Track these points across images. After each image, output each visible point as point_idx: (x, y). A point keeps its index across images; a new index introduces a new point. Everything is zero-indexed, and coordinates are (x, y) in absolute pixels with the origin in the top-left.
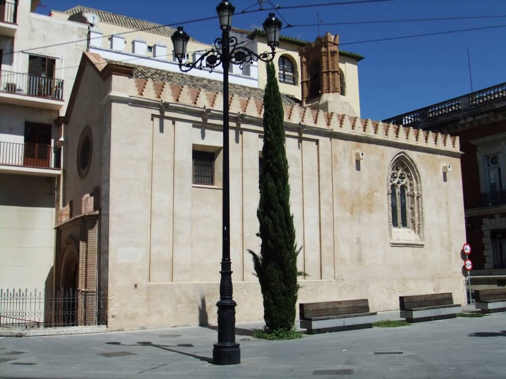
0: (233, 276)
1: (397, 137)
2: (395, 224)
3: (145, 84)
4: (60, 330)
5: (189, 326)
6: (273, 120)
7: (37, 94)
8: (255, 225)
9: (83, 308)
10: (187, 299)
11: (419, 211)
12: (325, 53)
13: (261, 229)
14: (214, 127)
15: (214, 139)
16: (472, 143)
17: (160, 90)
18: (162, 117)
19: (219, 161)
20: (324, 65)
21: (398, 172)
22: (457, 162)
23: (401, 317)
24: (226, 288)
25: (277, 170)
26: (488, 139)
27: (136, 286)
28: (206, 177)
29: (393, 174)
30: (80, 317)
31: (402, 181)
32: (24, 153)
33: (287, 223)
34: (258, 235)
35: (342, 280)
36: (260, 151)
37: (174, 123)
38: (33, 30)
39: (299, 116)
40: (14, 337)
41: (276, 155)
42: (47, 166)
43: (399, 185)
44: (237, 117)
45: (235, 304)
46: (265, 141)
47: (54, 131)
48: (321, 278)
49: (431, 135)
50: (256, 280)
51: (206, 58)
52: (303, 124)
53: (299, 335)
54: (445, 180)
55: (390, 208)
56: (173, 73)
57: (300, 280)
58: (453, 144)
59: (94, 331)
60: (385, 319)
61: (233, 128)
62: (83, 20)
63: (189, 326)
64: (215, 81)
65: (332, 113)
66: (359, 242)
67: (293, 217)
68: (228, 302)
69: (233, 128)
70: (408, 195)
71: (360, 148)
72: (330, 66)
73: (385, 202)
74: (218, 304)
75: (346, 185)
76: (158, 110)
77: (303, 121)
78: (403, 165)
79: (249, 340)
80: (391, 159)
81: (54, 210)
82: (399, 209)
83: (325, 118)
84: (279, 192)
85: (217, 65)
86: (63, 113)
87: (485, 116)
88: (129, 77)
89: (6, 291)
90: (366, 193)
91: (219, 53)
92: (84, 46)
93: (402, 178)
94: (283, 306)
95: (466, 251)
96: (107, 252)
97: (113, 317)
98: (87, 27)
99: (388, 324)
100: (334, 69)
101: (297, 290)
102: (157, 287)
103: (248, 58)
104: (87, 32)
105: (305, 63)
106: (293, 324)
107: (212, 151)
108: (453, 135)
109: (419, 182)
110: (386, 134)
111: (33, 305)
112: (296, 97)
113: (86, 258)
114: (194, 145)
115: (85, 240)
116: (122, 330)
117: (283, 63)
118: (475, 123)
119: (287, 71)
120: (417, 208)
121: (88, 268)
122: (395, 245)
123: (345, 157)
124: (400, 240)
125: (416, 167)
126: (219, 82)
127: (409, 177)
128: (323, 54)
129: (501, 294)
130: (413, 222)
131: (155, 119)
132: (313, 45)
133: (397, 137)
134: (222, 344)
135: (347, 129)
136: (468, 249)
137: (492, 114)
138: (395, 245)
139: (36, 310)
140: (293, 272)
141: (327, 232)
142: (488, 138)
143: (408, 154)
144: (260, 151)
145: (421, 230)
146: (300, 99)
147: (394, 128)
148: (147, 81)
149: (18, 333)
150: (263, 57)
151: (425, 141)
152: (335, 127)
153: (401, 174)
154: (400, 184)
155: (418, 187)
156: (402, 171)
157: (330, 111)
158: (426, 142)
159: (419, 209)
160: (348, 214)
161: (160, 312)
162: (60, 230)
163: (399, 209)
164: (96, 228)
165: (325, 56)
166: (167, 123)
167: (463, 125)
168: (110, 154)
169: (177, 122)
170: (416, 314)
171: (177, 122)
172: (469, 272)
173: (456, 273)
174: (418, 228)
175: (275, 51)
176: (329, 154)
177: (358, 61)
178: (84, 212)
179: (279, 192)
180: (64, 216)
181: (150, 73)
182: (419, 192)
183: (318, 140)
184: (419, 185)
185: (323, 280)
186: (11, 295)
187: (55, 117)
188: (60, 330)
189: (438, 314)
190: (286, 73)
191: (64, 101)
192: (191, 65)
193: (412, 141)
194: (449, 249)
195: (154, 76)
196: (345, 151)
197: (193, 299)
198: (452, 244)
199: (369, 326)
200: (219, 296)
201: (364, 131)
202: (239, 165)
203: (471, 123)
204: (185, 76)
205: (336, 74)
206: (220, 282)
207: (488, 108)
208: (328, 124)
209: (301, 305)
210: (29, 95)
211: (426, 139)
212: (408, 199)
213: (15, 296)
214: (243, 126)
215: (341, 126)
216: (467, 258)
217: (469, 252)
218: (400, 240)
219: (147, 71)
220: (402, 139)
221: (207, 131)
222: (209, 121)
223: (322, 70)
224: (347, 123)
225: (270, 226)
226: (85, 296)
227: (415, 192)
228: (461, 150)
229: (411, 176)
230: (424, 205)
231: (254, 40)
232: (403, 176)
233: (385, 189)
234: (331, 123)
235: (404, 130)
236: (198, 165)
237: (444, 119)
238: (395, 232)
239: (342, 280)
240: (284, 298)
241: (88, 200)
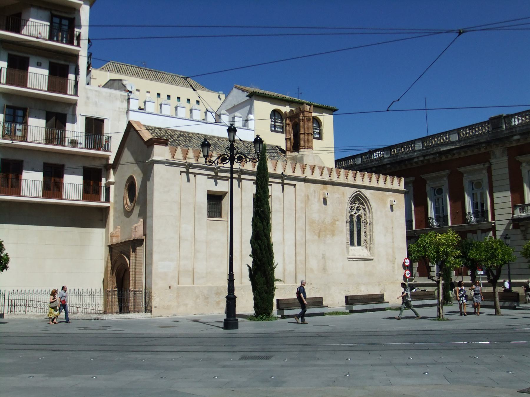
0: (234, 281)
1: (355, 180)
2: (352, 243)
3: (176, 150)
4: (122, 316)
5: (205, 314)
6: (262, 183)
7: (93, 147)
8: (248, 249)
9: (133, 302)
10: (203, 296)
13: (253, 252)
14: (224, 179)
15: (223, 186)
16: (423, 178)
17: (185, 154)
18: (188, 173)
19: (226, 202)
20: (302, 128)
21: (355, 205)
22: (402, 197)
23: (346, 309)
24: (231, 288)
25: (263, 215)
26: (434, 175)
27: (170, 287)
28: (216, 212)
29: (352, 207)
30: (131, 307)
31: (358, 212)
33: (268, 248)
34: (250, 256)
35: (311, 284)
36: (253, 194)
37: (195, 176)
38: (88, 98)
39: (282, 168)
41: (263, 206)
42: (99, 200)
43: (356, 215)
45: (236, 297)
46: (257, 187)
47: (103, 173)
48: (296, 283)
49: (382, 177)
50: (250, 283)
51: (220, 158)
52: (285, 173)
53: (276, 319)
54: (392, 210)
55: (349, 233)
56: (192, 133)
57: (276, 284)
58: (399, 184)
59: (143, 317)
60: (335, 311)
61: (236, 178)
62: (122, 87)
63: (205, 314)
64: (222, 138)
65: (306, 164)
66: (324, 257)
67: (272, 244)
68: (232, 296)
69: (236, 178)
71: (326, 189)
72: (306, 129)
73: (345, 228)
74: (227, 297)
75: (315, 216)
76: (185, 168)
77: (284, 171)
78: (359, 200)
79: (244, 321)
80: (350, 197)
81: (103, 230)
82: (355, 233)
83: (301, 168)
84: (264, 229)
85: (227, 163)
86: (111, 161)
87: (432, 156)
88: (165, 146)
89: (32, 291)
90: (330, 222)
91: (228, 156)
92: (125, 108)
93: (358, 209)
94: (265, 300)
95: (406, 264)
96: (151, 264)
97: (155, 307)
98: (127, 94)
99: (337, 313)
101: (274, 290)
102: (184, 288)
103: (244, 160)
104: (127, 98)
106: (272, 312)
107: (221, 194)
108: (399, 176)
109: (371, 213)
110: (347, 178)
112: (282, 148)
113: (135, 268)
114: (208, 191)
116: (161, 316)
117: (274, 116)
118: (425, 162)
119: (277, 122)
121: (137, 275)
122: (351, 259)
123: (314, 196)
124: (354, 256)
125: (369, 201)
126: (225, 138)
127: (363, 209)
129: (423, 295)
130: (366, 242)
131: (182, 174)
133: (355, 180)
134: (228, 319)
135: (316, 176)
136: (408, 262)
137: (438, 155)
138: (351, 259)
139: (98, 303)
140: (272, 279)
141: (300, 250)
142: (434, 174)
143: (363, 192)
144: (253, 194)
145: (371, 248)
146: (284, 148)
147: (353, 173)
148: (177, 148)
149: (96, 317)
150: (253, 160)
151: (377, 182)
152: (308, 175)
153: (358, 207)
154: (357, 214)
156: (359, 204)
157: (305, 163)
158: (378, 183)
160: (316, 237)
161: (186, 305)
162: (112, 248)
163: (355, 233)
165: (302, 121)
166: (191, 176)
167: (416, 163)
168: (153, 199)
169: (197, 176)
170: (355, 308)
171: (197, 176)
172: (407, 279)
173: (398, 280)
174: (369, 246)
176: (304, 194)
177: (333, 112)
179: (264, 229)
180: (114, 238)
181: (177, 136)
182: (371, 220)
183: (295, 185)
186: (89, 293)
188: (122, 316)
189: (372, 308)
190: (276, 124)
192: (212, 162)
193: (366, 183)
194: (393, 262)
195: (179, 138)
196: (315, 191)
197: (207, 296)
198: (395, 258)
199: (323, 314)
200: (227, 292)
201: (330, 176)
202: (239, 204)
203: (422, 161)
204: (201, 136)
205: (310, 135)
206: (228, 285)
207: (435, 150)
208: (303, 173)
209: (278, 300)
210: (86, 147)
211: (378, 181)
212: (362, 225)
213: (92, 293)
214: (243, 176)
215: (312, 174)
216: (407, 269)
217: (408, 264)
218: (354, 256)
219: (174, 133)
220: (359, 182)
221: (218, 181)
222: (220, 174)
223: (300, 132)
224: (317, 172)
225: (259, 250)
226: (135, 294)
227: (368, 220)
228: (405, 188)
229: (365, 208)
230: (375, 230)
231: (252, 97)
232: (359, 208)
233: (346, 217)
234: (305, 172)
235: (361, 174)
236: (211, 204)
237: (403, 156)
238: (352, 250)
239: (311, 284)
240: (266, 295)
241: (136, 228)
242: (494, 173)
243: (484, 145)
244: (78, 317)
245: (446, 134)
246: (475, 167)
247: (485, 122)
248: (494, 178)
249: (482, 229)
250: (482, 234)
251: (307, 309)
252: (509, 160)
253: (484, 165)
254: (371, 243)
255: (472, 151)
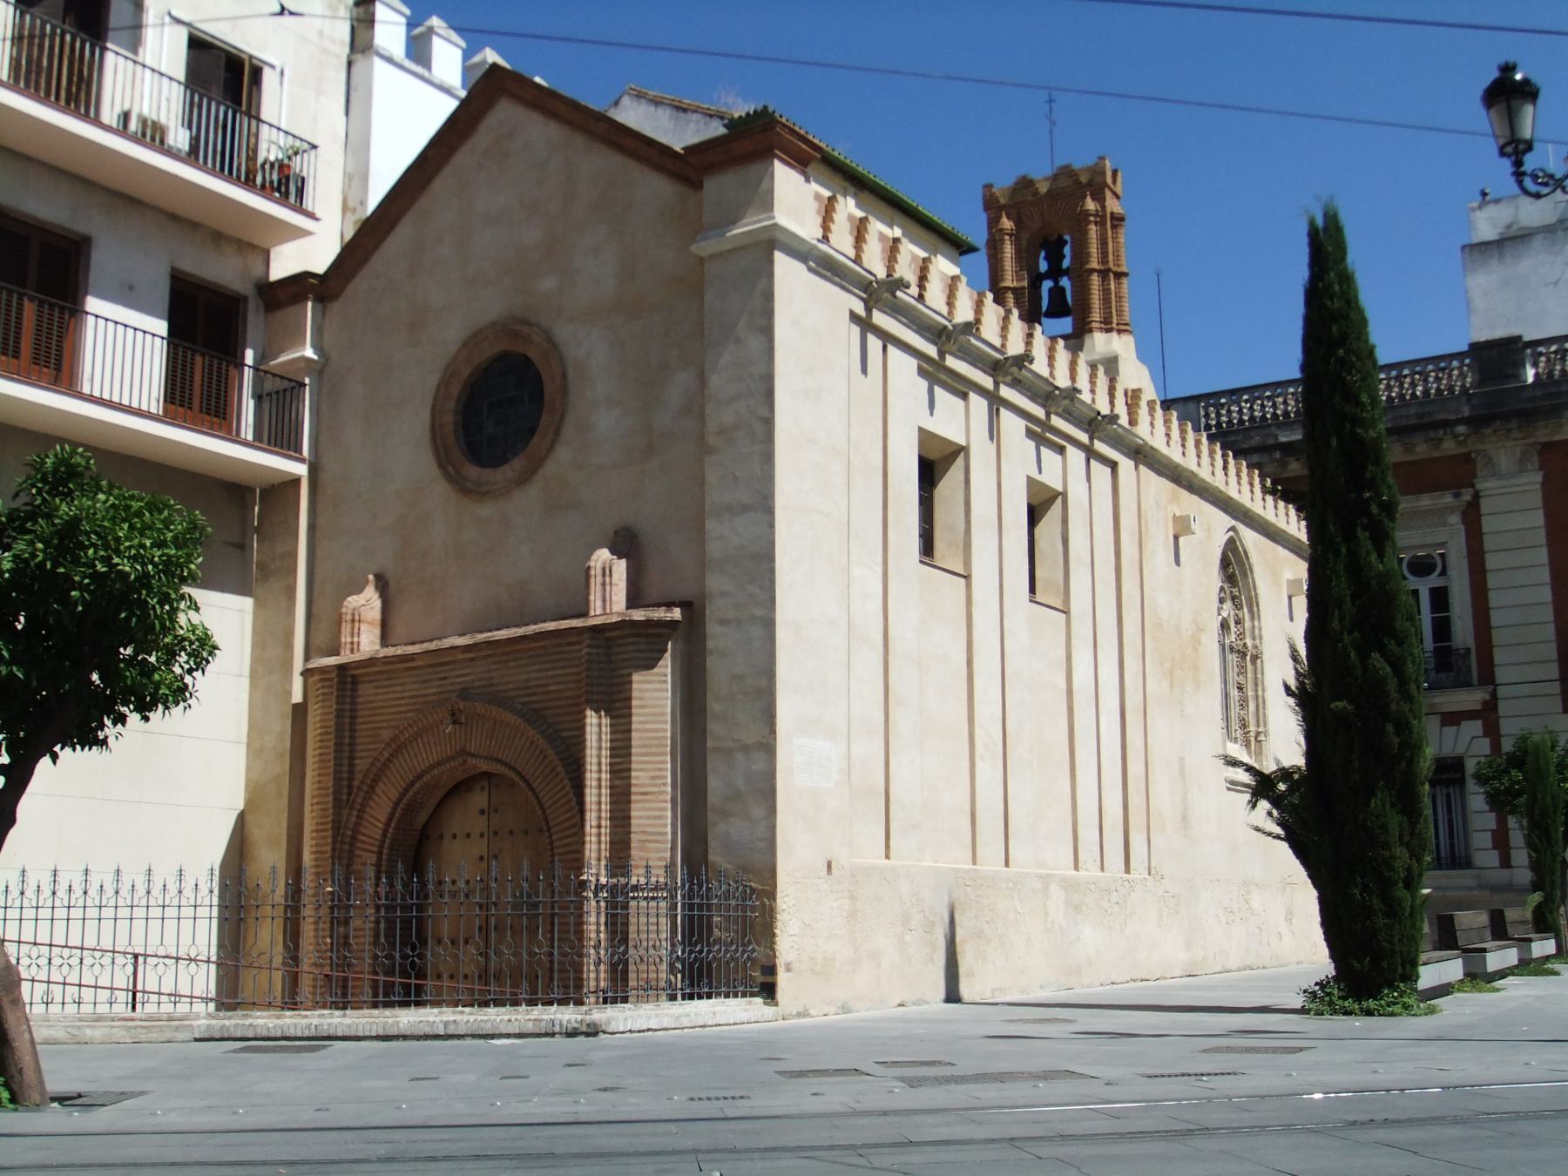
11: (1257, 697)
12: (1096, 215)
30: (595, 975)
32: (166, 387)
40: (559, 1040)
44: (1000, 361)
70: (1232, 649)
97: (788, 969)
100: (1118, 265)
105: (1011, 235)
111: (171, 925)
115: (618, 706)
120: (1253, 686)
128: (1092, 219)
132: (1043, 188)
137: (1278, 455)
155: (1253, 627)
159: (1256, 691)
162: (353, 676)
164: (666, 665)
175: (1522, 169)
177: (962, 254)
178: (599, 612)
182: (1257, 642)
184: (1256, 623)
185: (1082, 873)
187: (258, 271)
191: (921, 429)
227: (1249, 642)
242: (1487, 524)
243: (1461, 429)
244: (446, 1024)
245: (1199, 403)
246: (1421, 503)
247: (1452, 356)
248: (1489, 543)
249: (1443, 714)
250: (1445, 729)
251: (1422, 970)
252: (1543, 484)
253: (1457, 495)
254: (1261, 729)
255: (1409, 448)
